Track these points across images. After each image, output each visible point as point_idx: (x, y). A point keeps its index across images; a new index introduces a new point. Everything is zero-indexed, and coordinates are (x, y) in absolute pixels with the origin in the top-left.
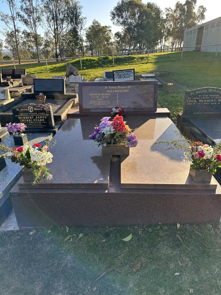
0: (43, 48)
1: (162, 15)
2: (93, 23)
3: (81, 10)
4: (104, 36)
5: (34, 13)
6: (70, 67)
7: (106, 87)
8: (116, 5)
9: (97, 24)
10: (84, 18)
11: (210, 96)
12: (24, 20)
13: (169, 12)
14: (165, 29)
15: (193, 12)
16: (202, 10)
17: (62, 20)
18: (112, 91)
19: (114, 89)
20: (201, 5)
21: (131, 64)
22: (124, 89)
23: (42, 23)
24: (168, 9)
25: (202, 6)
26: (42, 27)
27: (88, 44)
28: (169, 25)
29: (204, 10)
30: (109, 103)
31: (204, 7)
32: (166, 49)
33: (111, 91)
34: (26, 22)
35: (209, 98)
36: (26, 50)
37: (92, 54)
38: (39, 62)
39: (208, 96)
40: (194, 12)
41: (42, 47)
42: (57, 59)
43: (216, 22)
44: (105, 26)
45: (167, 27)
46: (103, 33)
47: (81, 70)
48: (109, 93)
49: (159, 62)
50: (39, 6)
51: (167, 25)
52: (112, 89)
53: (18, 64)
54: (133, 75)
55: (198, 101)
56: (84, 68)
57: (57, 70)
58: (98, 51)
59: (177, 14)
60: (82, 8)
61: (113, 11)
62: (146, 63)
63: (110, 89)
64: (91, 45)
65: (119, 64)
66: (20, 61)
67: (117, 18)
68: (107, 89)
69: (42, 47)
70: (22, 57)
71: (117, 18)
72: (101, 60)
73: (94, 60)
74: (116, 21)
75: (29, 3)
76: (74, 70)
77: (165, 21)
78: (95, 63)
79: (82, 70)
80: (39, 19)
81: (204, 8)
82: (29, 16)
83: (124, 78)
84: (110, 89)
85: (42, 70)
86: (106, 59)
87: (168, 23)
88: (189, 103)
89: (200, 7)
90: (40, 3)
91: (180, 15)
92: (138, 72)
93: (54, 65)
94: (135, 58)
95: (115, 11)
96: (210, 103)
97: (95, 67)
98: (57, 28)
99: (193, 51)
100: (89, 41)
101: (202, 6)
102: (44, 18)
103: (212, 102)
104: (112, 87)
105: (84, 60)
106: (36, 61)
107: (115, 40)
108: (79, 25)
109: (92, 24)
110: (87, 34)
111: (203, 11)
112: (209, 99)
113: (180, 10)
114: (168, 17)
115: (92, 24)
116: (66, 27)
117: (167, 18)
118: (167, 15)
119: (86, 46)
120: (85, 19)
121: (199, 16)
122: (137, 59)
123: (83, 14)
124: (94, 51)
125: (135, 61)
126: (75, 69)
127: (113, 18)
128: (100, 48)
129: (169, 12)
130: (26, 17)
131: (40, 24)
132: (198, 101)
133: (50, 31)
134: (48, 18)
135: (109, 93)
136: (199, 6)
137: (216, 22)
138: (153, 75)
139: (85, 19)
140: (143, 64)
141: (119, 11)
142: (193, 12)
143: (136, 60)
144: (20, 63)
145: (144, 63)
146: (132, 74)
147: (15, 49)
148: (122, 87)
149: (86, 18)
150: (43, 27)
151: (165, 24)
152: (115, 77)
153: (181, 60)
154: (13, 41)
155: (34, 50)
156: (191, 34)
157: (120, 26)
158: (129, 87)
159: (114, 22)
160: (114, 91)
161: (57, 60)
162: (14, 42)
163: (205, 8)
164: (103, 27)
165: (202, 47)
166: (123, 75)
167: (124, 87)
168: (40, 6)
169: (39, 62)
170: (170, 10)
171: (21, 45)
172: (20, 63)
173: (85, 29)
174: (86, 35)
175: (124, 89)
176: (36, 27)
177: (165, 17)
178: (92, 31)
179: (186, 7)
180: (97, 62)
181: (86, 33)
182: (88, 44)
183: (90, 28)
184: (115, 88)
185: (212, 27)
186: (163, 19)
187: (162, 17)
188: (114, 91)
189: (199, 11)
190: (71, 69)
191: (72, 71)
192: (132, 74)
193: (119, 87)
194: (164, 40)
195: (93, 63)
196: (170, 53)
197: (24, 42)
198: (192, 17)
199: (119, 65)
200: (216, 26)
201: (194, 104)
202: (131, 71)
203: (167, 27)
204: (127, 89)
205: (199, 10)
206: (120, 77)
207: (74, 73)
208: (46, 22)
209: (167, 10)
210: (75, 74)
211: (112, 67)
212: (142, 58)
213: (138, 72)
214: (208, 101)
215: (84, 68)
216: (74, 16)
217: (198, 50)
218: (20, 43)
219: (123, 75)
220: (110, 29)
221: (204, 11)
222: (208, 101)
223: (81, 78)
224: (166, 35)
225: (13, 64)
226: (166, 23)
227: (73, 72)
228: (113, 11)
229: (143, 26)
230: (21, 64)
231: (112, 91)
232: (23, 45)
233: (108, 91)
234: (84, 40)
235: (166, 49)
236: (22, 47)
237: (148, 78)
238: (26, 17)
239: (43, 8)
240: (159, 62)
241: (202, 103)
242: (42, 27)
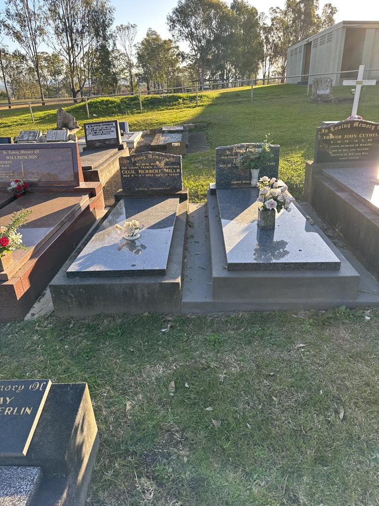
0: (64, 79)
1: (263, 19)
2: (148, 35)
3: (113, 13)
4: (166, 58)
5: (32, 21)
6: (64, 115)
7: (5, 152)
8: (176, 5)
9: (154, 37)
10: (131, 26)
11: (152, 164)
12: (14, 33)
13: (276, 15)
14: (270, 44)
15: (316, 14)
16: (330, 10)
17: (81, 33)
18: (14, 157)
19: (16, 155)
20: (328, 2)
21: (170, 108)
22: (30, 154)
23: (46, 38)
24: (275, 10)
25: (330, 5)
26: (48, 44)
27: (141, 71)
28: (277, 37)
29: (333, 11)
30: (11, 174)
31: (333, 6)
32: (277, 78)
33: (12, 158)
34: (18, 36)
35: (151, 167)
36: (35, 82)
37: (148, 89)
38: (43, 104)
39: (148, 164)
40: (317, 15)
41: (61, 77)
42: (75, 99)
43: (319, 39)
44: (168, 39)
45: (274, 41)
46: (164, 51)
47: (87, 119)
48: (10, 160)
49: (215, 104)
50: (41, 9)
51: (273, 37)
52: (14, 155)
53: (7, 108)
54: (115, 131)
55: (136, 171)
56: (94, 115)
57: (49, 119)
58: (158, 83)
59: (289, 19)
60: (114, 11)
61: (171, 14)
62: (196, 106)
63: (11, 155)
64: (145, 73)
65: (152, 109)
66: (10, 103)
67: (179, 27)
68: (6, 155)
69: (61, 77)
70: (28, 95)
71: (178, 26)
72: (125, 102)
73: (112, 102)
74: (177, 32)
75: (21, 5)
76: (70, 120)
77: (268, 30)
78: (115, 107)
79: (90, 119)
80: (41, 30)
81: (332, 8)
82: (23, 26)
83: (102, 134)
84: (11, 155)
85: (25, 120)
86: (134, 100)
87: (274, 33)
88: (125, 174)
89: (326, 6)
90: (42, 3)
91: (294, 21)
92: (165, 123)
93: (47, 112)
94: (180, 98)
95: (174, 15)
96: (145, 174)
97: (113, 113)
98: (73, 46)
99: (298, 83)
100: (143, 67)
101: (330, 5)
102: (50, 29)
103: (157, 173)
104: (13, 152)
105: (98, 102)
106: (70, 100)
107: (187, 64)
108: (111, 42)
109: (146, 37)
110: (138, 53)
111: (331, 12)
112: (151, 169)
113: (294, 11)
114: (275, 23)
115: (146, 37)
116: (88, 43)
117: (273, 24)
118: (272, 20)
119: (136, 75)
120: (134, 27)
121: (325, 21)
122: (184, 100)
123: (118, 20)
124: (151, 83)
125: (179, 103)
126: (71, 118)
127: (173, 27)
128: (160, 77)
129: (276, 15)
130: (18, 28)
131: (44, 40)
132: (136, 171)
133: (61, 52)
134: (57, 28)
135: (10, 160)
136: (324, 5)
137: (319, 39)
138: (181, 128)
139: (134, 27)
140: (189, 109)
141: (181, 16)
142: (316, 14)
143: (181, 101)
144: (10, 107)
145: (190, 107)
146: (112, 129)
147: (15, 80)
148: (27, 152)
149: (136, 26)
150: (49, 45)
151: (270, 36)
152: (87, 134)
153: (252, 101)
154: (11, 67)
155: (48, 83)
156: (296, 54)
157: (185, 41)
158: (37, 151)
159: (174, 34)
160: (17, 157)
161: (74, 100)
162: (14, 69)
163: (335, 8)
164: (165, 41)
165: (309, 78)
166: (100, 130)
167: (29, 152)
168: (43, 9)
169: (43, 104)
170: (278, 10)
171: (26, 74)
172: (10, 107)
173: (135, 46)
174: (137, 56)
175: (30, 154)
176: (35, 44)
177: (269, 23)
178: (146, 49)
179: (302, 6)
180: (119, 106)
181: (136, 52)
182: (141, 71)
183: (143, 44)
184: (18, 153)
185: (322, 43)
186: (266, 26)
187: (264, 24)
188: (17, 157)
189: (324, 14)
190: (65, 118)
191: (67, 121)
192: (112, 129)
193: (22, 152)
194: (268, 62)
195: (110, 107)
196: (260, 86)
197: (30, 68)
198: (312, 24)
199: (151, 111)
200: (326, 41)
201: (133, 176)
202: (112, 124)
203: (274, 41)
204: (34, 154)
205: (324, 12)
206: (95, 133)
207: (69, 125)
208: (55, 36)
209: (273, 11)
210: (72, 125)
211: (139, 113)
212: (193, 99)
213: (165, 123)
214: (150, 171)
215: (94, 115)
216: (98, 23)
217: (304, 82)
218: (23, 71)
219: (100, 130)
220: (177, 45)
221: (332, 13)
222: (150, 171)
223: (65, 133)
224: (273, 54)
225: (27, 106)
226: (271, 34)
227: (69, 123)
228: (171, 14)
229: (231, 42)
230: (12, 107)
231: (14, 157)
232: (29, 74)
233: (8, 158)
234: (135, 64)
235: (277, 78)
236: (27, 77)
237: (171, 133)
238: (18, 28)
239: (48, 12)
240: (215, 104)
241: (143, 174)
242: (48, 44)
